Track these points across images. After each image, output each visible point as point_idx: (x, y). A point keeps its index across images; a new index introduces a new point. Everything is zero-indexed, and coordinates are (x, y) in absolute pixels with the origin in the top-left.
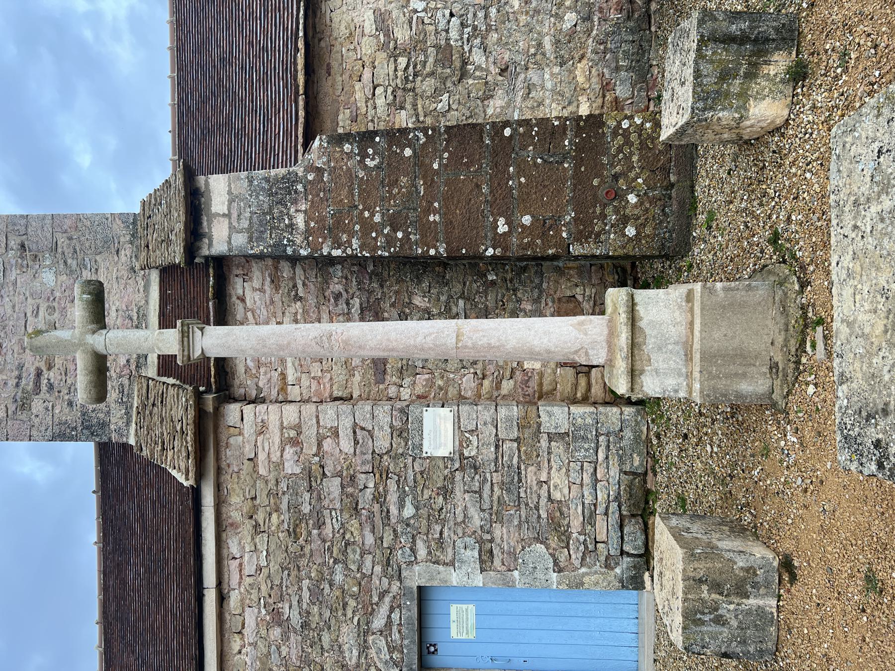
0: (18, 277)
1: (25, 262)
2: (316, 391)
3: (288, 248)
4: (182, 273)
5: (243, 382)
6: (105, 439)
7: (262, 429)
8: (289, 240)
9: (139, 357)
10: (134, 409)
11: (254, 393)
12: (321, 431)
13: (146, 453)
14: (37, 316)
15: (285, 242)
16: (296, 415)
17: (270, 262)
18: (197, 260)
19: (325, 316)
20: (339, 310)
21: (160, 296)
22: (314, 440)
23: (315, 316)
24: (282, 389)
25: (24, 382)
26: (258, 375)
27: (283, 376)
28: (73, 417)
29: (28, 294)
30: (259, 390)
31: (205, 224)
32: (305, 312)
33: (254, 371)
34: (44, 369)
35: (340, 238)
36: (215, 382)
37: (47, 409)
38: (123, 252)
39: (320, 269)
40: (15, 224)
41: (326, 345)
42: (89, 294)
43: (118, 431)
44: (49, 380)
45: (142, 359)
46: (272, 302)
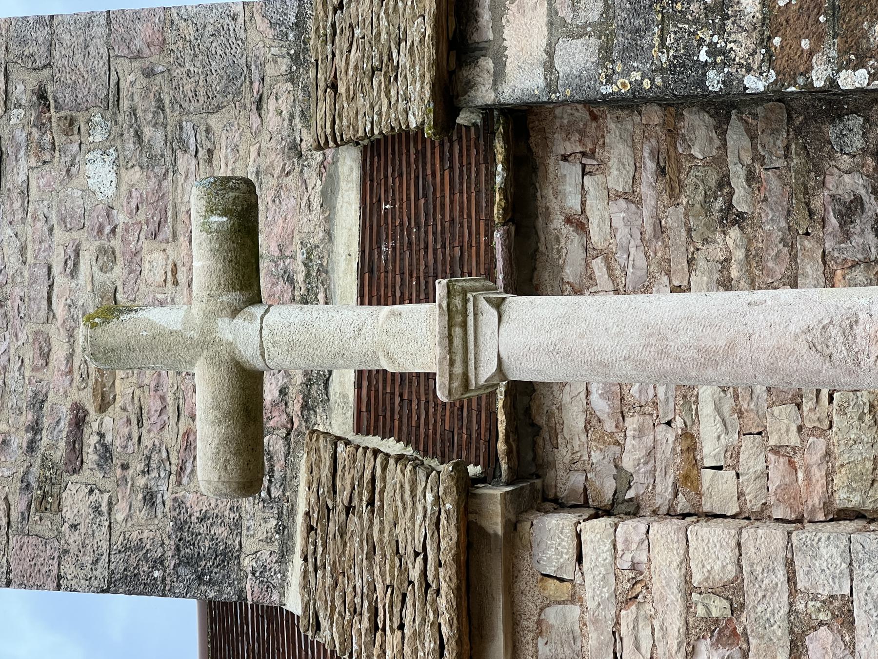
0: (33, 175)
1: (48, 137)
2: (784, 487)
3: (711, 74)
4: (421, 154)
5: (579, 455)
6: (229, 594)
7: (633, 589)
8: (713, 51)
9: (309, 382)
10: (300, 519)
11: (608, 487)
12: (800, 607)
13: (328, 635)
14: (74, 273)
15: (703, 57)
16: (728, 555)
17: (654, 115)
18: (463, 119)
19: (811, 268)
20: (852, 250)
21: (363, 217)
22: (779, 631)
23: (779, 270)
24: (686, 478)
25: (45, 439)
26: (619, 437)
27: (689, 442)
28: (154, 532)
29: (54, 219)
30: (624, 478)
31: (486, 16)
32: (753, 257)
33: (609, 426)
34: (91, 407)
35: (865, 35)
36: (509, 453)
37: (97, 509)
38: (271, 105)
39: (798, 132)
40: (24, 42)
41: (840, 352)
42: (225, 213)
43: (260, 573)
44: (102, 435)
45: (318, 382)
46: (660, 230)
